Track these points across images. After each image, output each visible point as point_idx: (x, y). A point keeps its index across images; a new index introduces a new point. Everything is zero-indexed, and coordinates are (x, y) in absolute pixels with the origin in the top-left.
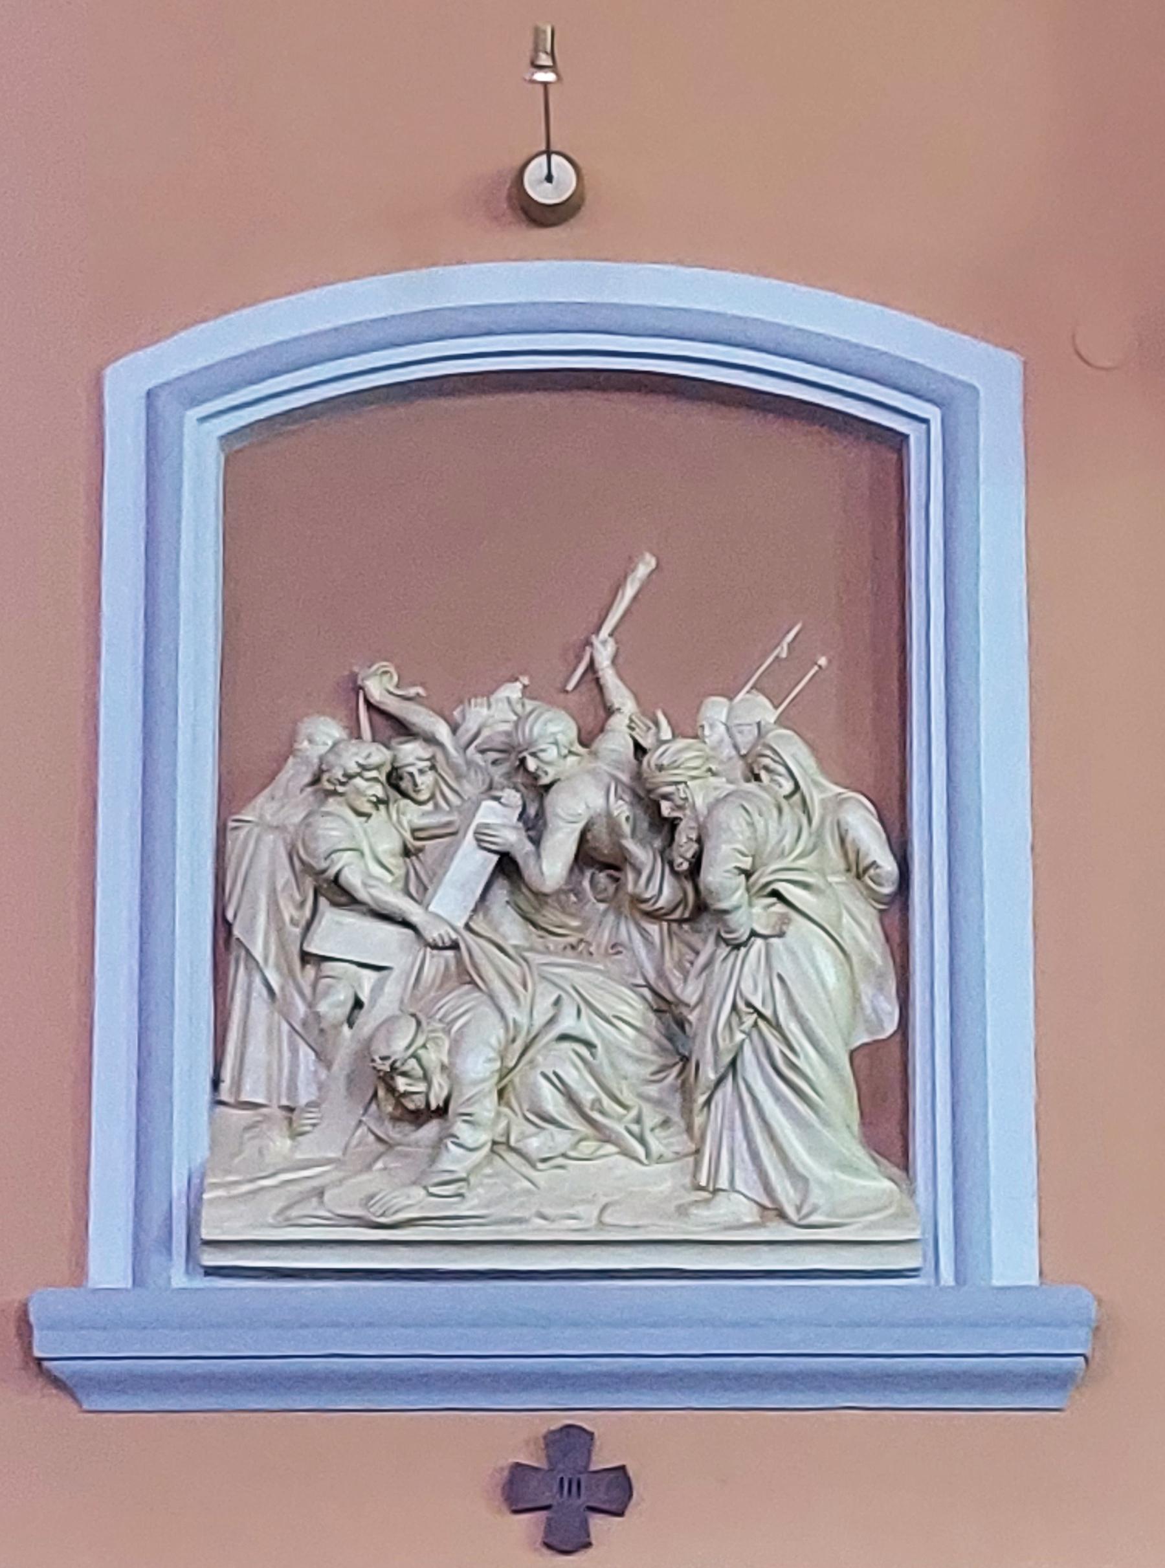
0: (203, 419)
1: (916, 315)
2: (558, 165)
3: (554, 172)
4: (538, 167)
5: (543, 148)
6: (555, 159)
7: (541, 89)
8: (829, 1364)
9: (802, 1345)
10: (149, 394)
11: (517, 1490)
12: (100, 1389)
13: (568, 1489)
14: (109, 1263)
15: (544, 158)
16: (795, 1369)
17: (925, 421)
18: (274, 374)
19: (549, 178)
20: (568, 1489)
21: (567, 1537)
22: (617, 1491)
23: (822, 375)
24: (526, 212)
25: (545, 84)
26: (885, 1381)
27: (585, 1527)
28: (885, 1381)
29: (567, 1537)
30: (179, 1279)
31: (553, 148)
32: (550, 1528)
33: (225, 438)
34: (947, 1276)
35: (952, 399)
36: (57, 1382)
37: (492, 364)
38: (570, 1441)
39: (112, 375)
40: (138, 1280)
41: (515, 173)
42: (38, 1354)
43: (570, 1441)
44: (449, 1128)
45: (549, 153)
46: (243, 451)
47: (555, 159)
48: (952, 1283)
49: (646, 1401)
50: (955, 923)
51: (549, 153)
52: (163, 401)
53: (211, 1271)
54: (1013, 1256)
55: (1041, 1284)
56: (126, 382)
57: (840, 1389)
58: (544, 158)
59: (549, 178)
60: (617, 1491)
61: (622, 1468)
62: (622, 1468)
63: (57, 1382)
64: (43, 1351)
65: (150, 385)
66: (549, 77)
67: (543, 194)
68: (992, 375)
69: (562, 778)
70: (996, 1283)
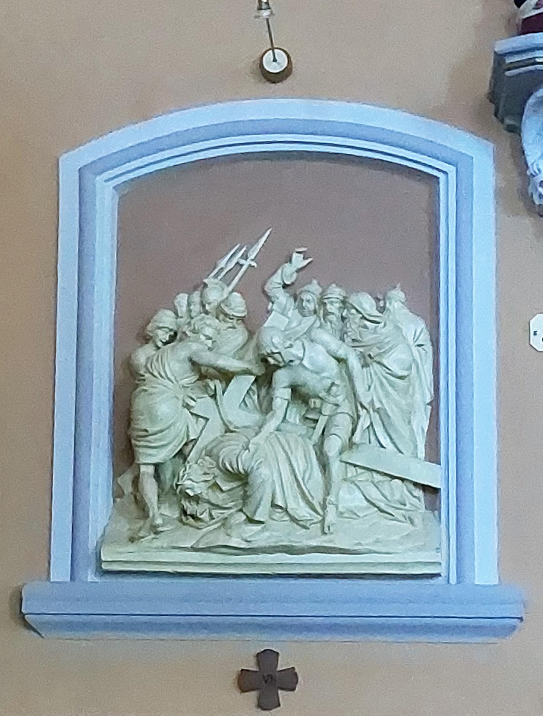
0: (106, 181)
2: (278, 54)
3: (277, 57)
4: (269, 56)
5: (270, 47)
6: (276, 51)
10: (79, 170)
11: (244, 681)
14: (60, 572)
15: (271, 52)
16: (488, 624)
19: (275, 60)
20: (266, 680)
21: (267, 702)
22: (290, 680)
24: (265, 77)
28: (428, 629)
29: (267, 702)
30: (91, 577)
31: (275, 46)
32: (259, 699)
34: (453, 579)
37: (278, 147)
38: (267, 657)
40: (72, 578)
43: (267, 657)
45: (273, 49)
47: (276, 51)
49: (454, 639)
50: (446, 407)
51: (273, 49)
52: (88, 175)
54: (485, 571)
56: (70, 163)
58: (271, 52)
59: (275, 60)
60: (290, 680)
63: (28, 626)
67: (272, 68)
70: (476, 584)
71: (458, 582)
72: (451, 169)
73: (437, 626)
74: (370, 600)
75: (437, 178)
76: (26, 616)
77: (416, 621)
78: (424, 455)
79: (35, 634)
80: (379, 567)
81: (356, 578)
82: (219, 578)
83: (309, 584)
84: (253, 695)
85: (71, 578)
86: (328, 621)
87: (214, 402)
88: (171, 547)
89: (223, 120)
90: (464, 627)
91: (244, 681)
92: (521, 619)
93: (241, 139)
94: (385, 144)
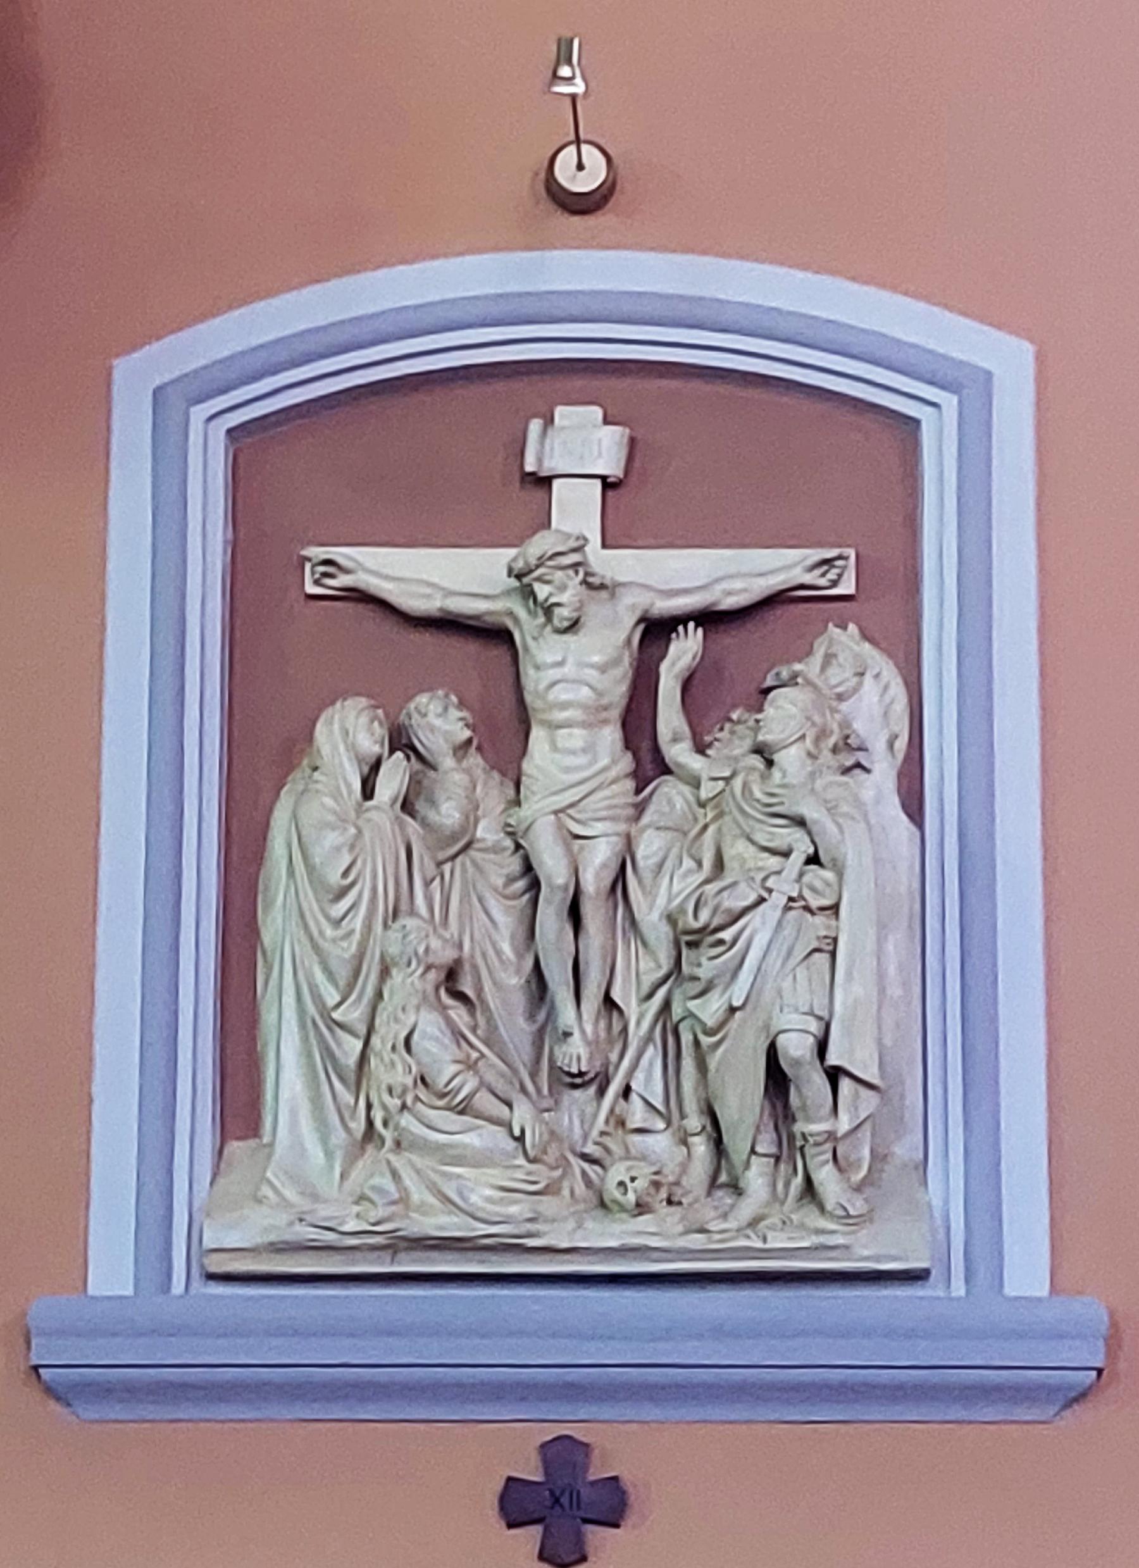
5: (572, 137)
7: (568, 103)
8: (80, 1374)
9: (47, 1356)
11: (517, 1505)
13: (563, 1502)
15: (572, 149)
18: (179, 876)
19: (580, 167)
20: (563, 1502)
22: (612, 1506)
25: (573, 97)
27: (579, 1540)
28: (180, 1392)
31: (582, 136)
33: (230, 431)
35: (971, 386)
38: (564, 1454)
39: (122, 368)
43: (564, 1454)
44: (673, 1134)
45: (578, 141)
47: (585, 148)
49: (700, 1413)
51: (578, 141)
53: (212, 1277)
54: (1027, 1271)
55: (968, 1292)
57: (788, 1402)
58: (572, 149)
59: (580, 167)
61: (510, 1479)
62: (615, 1479)
63: (50, 1391)
64: (39, 1358)
65: (158, 382)
66: (579, 87)
67: (584, 184)
68: (136, 377)
72: (948, 401)
73: (460, 1385)
74: (435, 1331)
75: (917, 422)
76: (41, 1371)
81: (687, 1281)
82: (338, 1284)
83: (859, 1297)
89: (913, 339)
90: (299, 1386)
91: (517, 1505)
92: (1100, 1371)
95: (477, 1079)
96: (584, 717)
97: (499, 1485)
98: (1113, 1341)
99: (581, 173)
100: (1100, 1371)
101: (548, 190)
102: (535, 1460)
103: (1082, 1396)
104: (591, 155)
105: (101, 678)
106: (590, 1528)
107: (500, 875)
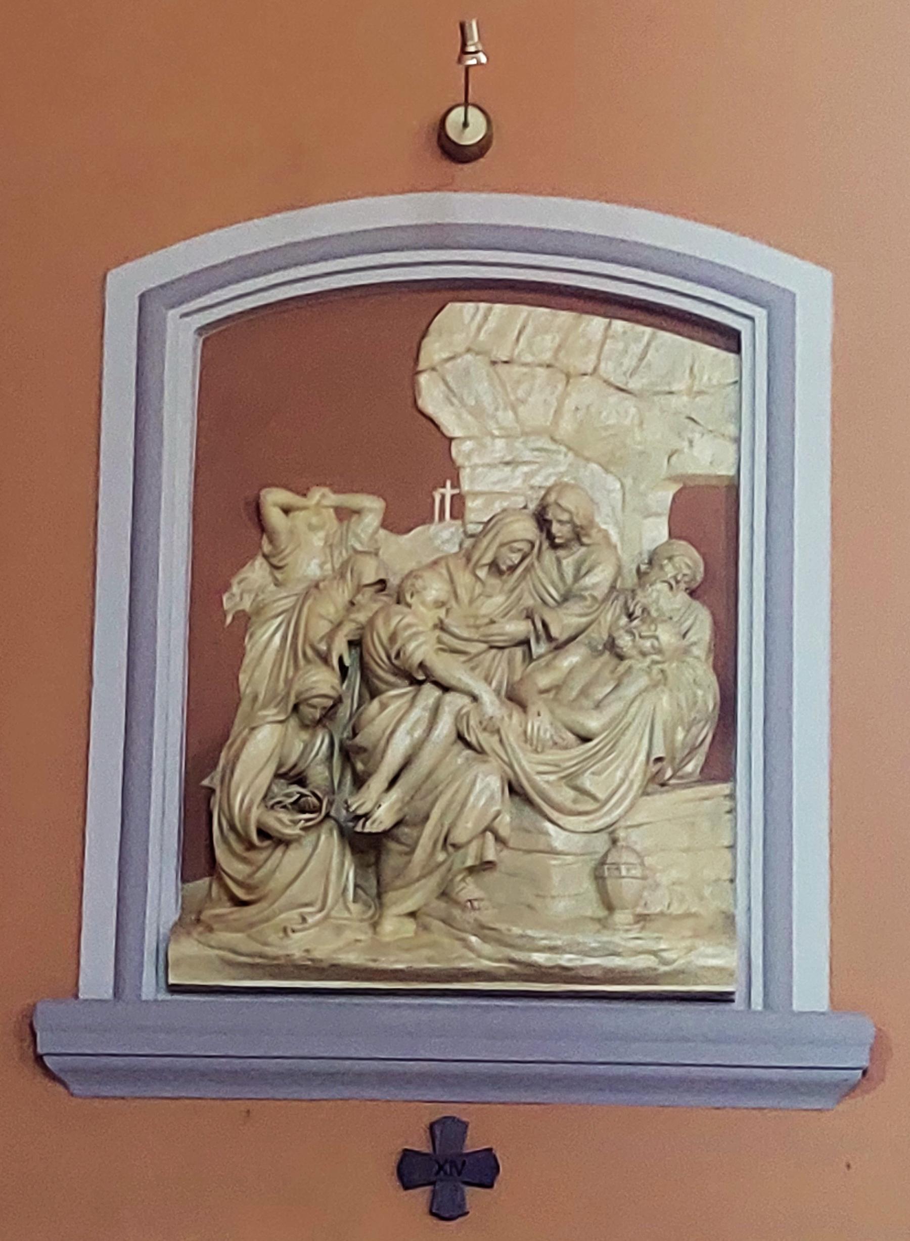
1: (162, 419)
4: (457, 115)
6: (472, 111)
11: (410, 1170)
12: (611, 1091)
13: (446, 1170)
14: (96, 976)
17: (751, 319)
19: (465, 124)
20: (446, 1170)
22: (485, 1170)
23: (639, 291)
26: (133, 1075)
28: (332, 1077)
31: (470, 100)
33: (201, 330)
36: (48, 1072)
38: (447, 1130)
39: (114, 278)
41: (439, 117)
42: (40, 1050)
43: (447, 1130)
45: (466, 104)
46: (217, 340)
48: (760, 1008)
51: (466, 104)
52: (152, 306)
56: (125, 284)
58: (460, 111)
59: (465, 124)
60: (485, 1170)
63: (48, 1072)
67: (472, 137)
69: (413, 608)
71: (766, 1005)
72: (760, 314)
76: (46, 1059)
77: (94, 1062)
78: (724, 786)
79: (61, 1089)
80: (503, 972)
84: (422, 1195)
85: (115, 994)
86: (94, 1062)
87: (458, 695)
88: (397, 939)
91: (410, 1170)
93: (568, 262)
94: (593, 258)
95: (427, 575)
96: (268, 888)
97: (395, 1159)
98: (880, 1048)
99: (468, 128)
100: (865, 1073)
101: (442, 147)
102: (425, 1136)
103: (853, 1088)
104: (475, 116)
105: (831, 792)
106: (468, 1190)
107: (493, 445)
